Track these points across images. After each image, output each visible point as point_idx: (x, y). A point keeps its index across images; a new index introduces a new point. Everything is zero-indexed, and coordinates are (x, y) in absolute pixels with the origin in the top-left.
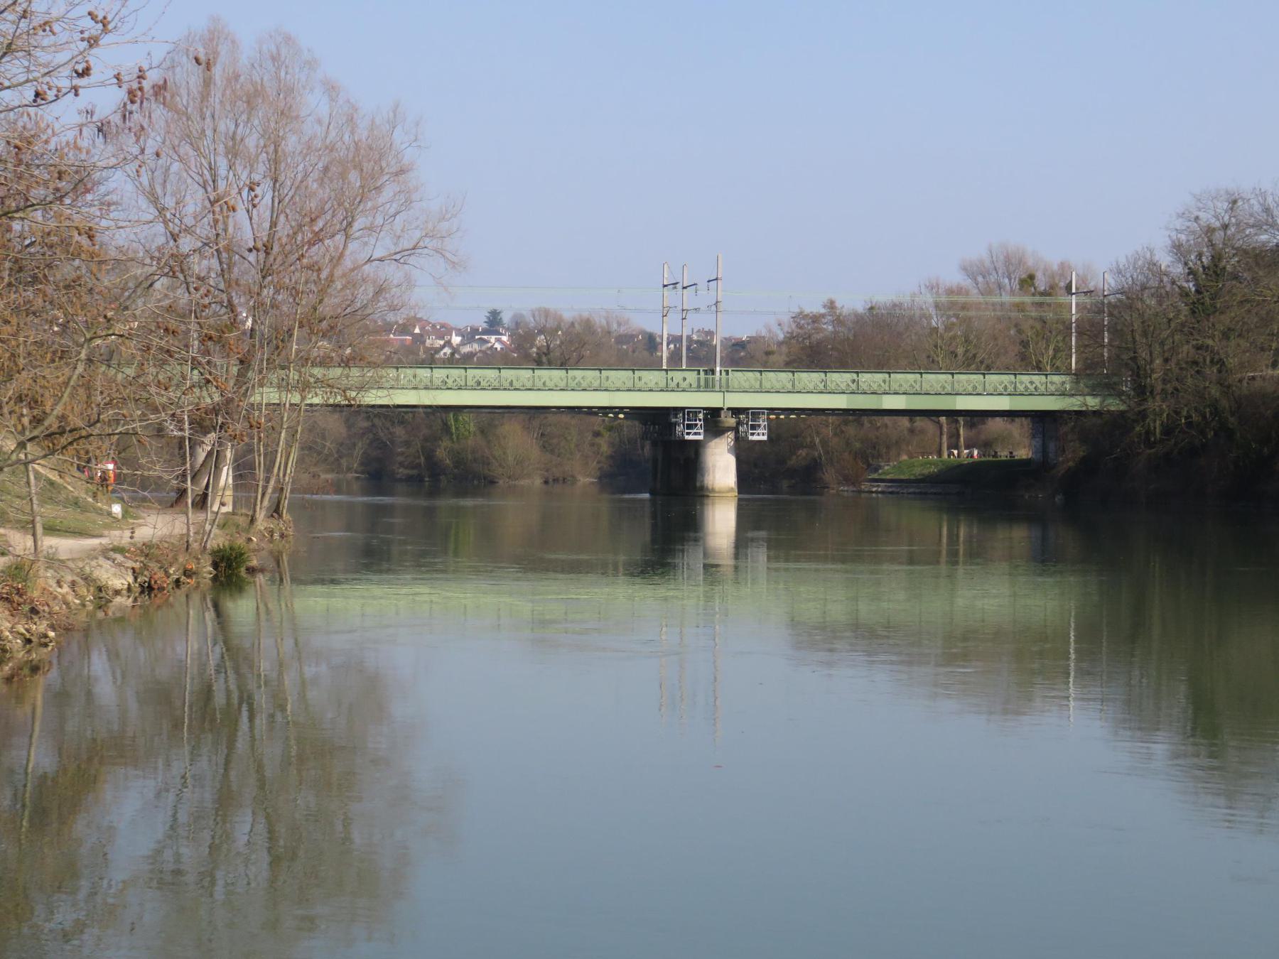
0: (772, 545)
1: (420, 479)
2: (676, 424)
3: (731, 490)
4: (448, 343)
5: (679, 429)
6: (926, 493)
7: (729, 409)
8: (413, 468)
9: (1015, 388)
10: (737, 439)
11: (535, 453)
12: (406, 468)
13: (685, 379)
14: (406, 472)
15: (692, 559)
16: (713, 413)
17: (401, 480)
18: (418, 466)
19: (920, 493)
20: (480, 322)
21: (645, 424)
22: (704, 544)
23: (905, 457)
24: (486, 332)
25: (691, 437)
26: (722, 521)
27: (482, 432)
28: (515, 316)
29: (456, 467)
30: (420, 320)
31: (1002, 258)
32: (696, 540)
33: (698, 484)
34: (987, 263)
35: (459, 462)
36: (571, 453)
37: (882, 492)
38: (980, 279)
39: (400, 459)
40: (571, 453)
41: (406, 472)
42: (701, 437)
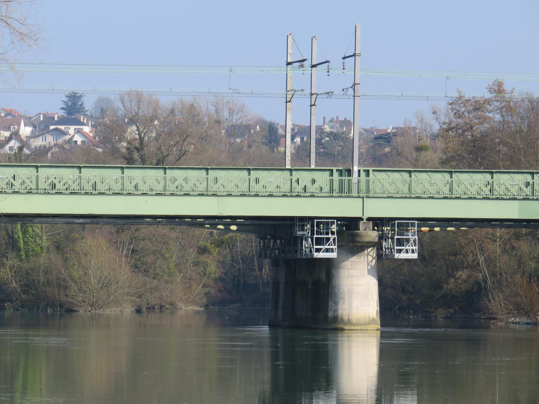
2: (302, 238)
3: (372, 321)
4: (16, 135)
7: (369, 219)
10: (379, 257)
11: (124, 274)
16: (349, 225)
21: (263, 238)
24: (62, 121)
27: (58, 248)
28: (100, 101)
29: (24, 292)
33: (330, 314)
35: (28, 285)
36: (170, 275)
42: (333, 255)
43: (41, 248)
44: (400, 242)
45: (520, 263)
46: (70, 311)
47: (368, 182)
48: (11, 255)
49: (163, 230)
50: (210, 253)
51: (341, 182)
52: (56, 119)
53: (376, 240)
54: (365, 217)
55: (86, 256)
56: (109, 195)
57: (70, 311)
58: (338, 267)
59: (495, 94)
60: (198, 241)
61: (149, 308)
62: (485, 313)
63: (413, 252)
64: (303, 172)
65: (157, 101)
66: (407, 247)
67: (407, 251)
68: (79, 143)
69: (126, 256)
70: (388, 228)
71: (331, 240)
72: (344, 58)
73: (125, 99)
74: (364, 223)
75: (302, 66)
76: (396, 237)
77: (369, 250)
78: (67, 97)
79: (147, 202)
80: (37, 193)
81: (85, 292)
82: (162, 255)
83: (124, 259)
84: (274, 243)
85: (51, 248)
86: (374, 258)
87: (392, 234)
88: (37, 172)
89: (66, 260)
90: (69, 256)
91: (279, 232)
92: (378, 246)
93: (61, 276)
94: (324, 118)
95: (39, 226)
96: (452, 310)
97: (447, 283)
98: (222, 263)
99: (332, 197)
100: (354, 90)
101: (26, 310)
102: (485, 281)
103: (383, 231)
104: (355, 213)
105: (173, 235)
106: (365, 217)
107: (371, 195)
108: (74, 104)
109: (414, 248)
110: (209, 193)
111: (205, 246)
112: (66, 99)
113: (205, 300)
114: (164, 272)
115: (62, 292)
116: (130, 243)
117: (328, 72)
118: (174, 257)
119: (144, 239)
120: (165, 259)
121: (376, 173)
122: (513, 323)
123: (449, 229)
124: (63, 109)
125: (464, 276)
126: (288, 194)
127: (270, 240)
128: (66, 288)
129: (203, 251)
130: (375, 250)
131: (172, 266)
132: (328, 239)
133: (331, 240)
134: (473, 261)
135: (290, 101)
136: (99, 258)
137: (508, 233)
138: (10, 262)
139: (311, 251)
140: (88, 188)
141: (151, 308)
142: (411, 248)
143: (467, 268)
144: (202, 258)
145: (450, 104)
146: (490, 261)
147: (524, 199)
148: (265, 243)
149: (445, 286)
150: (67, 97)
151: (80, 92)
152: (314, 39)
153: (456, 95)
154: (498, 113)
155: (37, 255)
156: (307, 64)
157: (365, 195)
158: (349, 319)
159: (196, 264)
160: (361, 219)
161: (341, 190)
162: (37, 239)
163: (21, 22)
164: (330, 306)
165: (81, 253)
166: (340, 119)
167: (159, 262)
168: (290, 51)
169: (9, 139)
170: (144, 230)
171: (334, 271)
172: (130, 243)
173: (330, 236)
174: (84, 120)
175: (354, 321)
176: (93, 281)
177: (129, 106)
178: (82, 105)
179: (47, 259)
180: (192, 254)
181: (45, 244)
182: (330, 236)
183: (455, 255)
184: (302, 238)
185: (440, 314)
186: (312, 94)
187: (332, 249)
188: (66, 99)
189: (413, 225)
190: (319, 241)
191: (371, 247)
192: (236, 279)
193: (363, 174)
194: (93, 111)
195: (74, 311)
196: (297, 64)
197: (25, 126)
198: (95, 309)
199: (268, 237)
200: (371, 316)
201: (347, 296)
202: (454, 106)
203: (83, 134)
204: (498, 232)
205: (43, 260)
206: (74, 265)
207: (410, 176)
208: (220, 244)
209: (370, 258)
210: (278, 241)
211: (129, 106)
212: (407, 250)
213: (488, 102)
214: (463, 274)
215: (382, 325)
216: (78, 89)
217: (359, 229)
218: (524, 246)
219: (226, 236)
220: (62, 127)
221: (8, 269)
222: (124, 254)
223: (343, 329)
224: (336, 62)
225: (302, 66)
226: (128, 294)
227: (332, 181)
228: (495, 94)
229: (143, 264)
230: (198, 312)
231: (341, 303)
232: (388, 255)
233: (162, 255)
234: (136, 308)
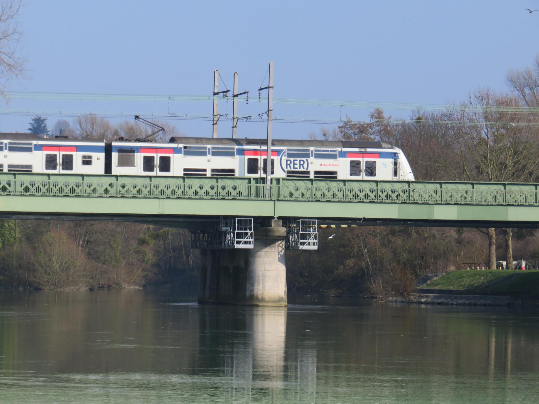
2: (225, 233)
3: (280, 300)
6: (475, 305)
7: (279, 218)
10: (287, 248)
11: (81, 261)
16: (262, 223)
19: (470, 305)
20: (25, 129)
21: (194, 233)
26: (271, 330)
28: (59, 123)
32: (246, 345)
33: (248, 293)
36: (116, 261)
37: (432, 303)
38: (527, 91)
42: (251, 246)
43: (15, 239)
44: (304, 237)
45: (396, 254)
46: (38, 289)
47: (278, 188)
49: (111, 226)
50: (148, 244)
51: (257, 189)
53: (285, 234)
54: (276, 217)
55: (51, 246)
56: (73, 197)
57: (38, 289)
59: (376, 120)
60: (138, 234)
61: (99, 287)
62: (368, 293)
63: (314, 244)
64: (227, 180)
65: (108, 123)
66: (309, 241)
67: (309, 244)
70: (295, 225)
71: (249, 234)
72: (260, 90)
73: (82, 122)
74: (275, 221)
75: (226, 96)
76: (301, 232)
77: (279, 242)
78: (33, 120)
79: (102, 203)
80: (15, 195)
81: (49, 274)
82: (110, 245)
83: (80, 248)
84: (203, 236)
85: (23, 239)
86: (283, 249)
87: (297, 230)
88: (15, 178)
89: (35, 249)
90: (37, 245)
92: (286, 239)
93: (31, 261)
95: (13, 221)
96: (341, 291)
97: (337, 269)
98: (157, 252)
100: (268, 115)
102: (368, 269)
103: (290, 227)
104: (270, 214)
105: (119, 230)
106: (276, 217)
107: (280, 199)
108: (39, 126)
109: (315, 241)
110: (443, 202)
111: (144, 239)
112: (32, 122)
113: (143, 282)
114: (112, 258)
116: (86, 236)
117: (247, 100)
118: (120, 248)
119: (96, 232)
120: (113, 248)
121: (284, 181)
122: (391, 301)
123: (342, 226)
124: (30, 129)
125: (352, 264)
126: (214, 197)
127: (200, 234)
128: (34, 271)
129: (143, 242)
130: (284, 243)
131: (118, 254)
132: (247, 234)
133: (249, 234)
134: (358, 252)
135: (216, 124)
136: (61, 248)
137: (386, 231)
139: (233, 243)
140: (522, 200)
141: (101, 287)
142: (312, 241)
143: (353, 257)
144: (142, 248)
145: (340, 127)
146: (372, 253)
147: (402, 203)
148: (195, 237)
149: (336, 271)
150: (33, 120)
152: (236, 74)
153: (345, 119)
154: (378, 135)
155: (11, 245)
156: (230, 94)
157: (276, 199)
158: (262, 297)
159: (137, 252)
160: (273, 218)
161: (257, 195)
162: (12, 232)
163: (9, 55)
164: (247, 287)
165: (46, 243)
167: (108, 251)
168: (216, 84)
170: (97, 225)
172: (86, 236)
173: (248, 231)
175: (267, 299)
176: (56, 266)
177: (85, 127)
178: (45, 126)
180: (134, 245)
181: (18, 235)
182: (248, 231)
183: (344, 247)
184: (225, 233)
185: (332, 293)
186: (234, 118)
187: (250, 241)
188: (32, 122)
189: (314, 223)
190: (239, 235)
191: (280, 240)
192: (168, 265)
193: (274, 182)
194: (54, 132)
195: (40, 289)
196: (222, 94)
198: (57, 288)
199: (199, 232)
200: (280, 295)
201: (261, 278)
202: (343, 129)
204: (378, 229)
205: (16, 248)
206: (41, 252)
207: (312, 184)
208: (156, 237)
209: (280, 249)
210: (206, 235)
211: (85, 127)
212: (309, 243)
213: (370, 126)
214: (350, 262)
215: (288, 303)
216: (40, 112)
217: (271, 226)
218: (398, 241)
219: (161, 231)
222: (81, 244)
223: (258, 306)
224: (254, 93)
225: (226, 96)
227: (249, 188)
228: (376, 120)
229: (96, 252)
230: (139, 290)
231: (256, 284)
232: (294, 247)
233: (110, 245)
234: (90, 287)
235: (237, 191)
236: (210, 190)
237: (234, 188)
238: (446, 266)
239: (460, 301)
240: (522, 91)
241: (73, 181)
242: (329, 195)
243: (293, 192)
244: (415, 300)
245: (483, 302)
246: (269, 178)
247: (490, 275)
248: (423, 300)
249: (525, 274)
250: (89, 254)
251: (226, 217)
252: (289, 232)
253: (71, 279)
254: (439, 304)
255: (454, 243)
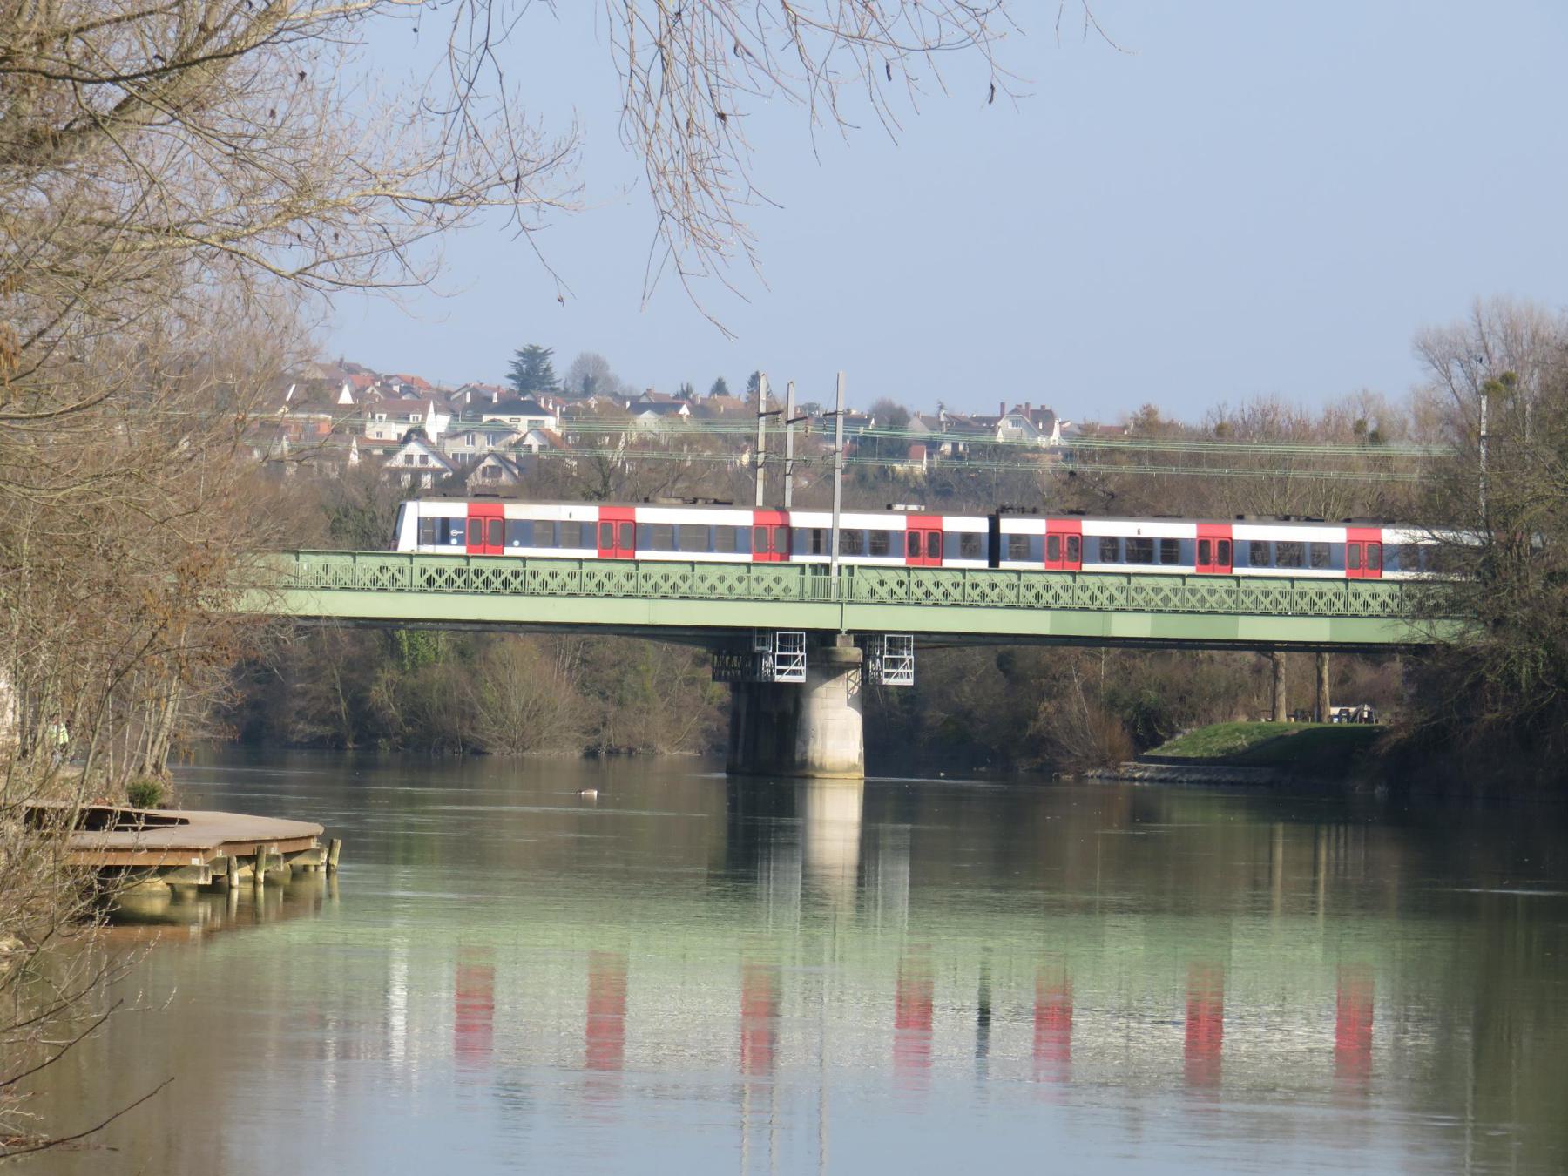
0: (917, 854)
1: (338, 743)
2: (762, 655)
3: (852, 768)
4: (418, 433)
5: (768, 664)
6: (1217, 783)
7: (849, 632)
8: (324, 722)
9: (1346, 604)
10: (865, 680)
11: (564, 696)
12: (311, 722)
13: (777, 580)
14: (308, 729)
15: (781, 879)
16: (821, 640)
17: (300, 746)
18: (334, 718)
19: (1208, 782)
20: (498, 377)
21: (719, 654)
22: (805, 852)
23: (1242, 719)
24: (511, 405)
25: (784, 678)
26: (836, 816)
27: (462, 653)
28: (582, 362)
29: (409, 722)
30: (353, 370)
31: (1498, 327)
32: (792, 845)
33: (798, 757)
34: (1472, 339)
35: (415, 712)
36: (646, 699)
37: (1151, 780)
38: (1456, 369)
39: (299, 703)
40: (646, 699)
41: (308, 729)
42: (801, 679)
48: (389, 664)
52: (495, 401)
54: (844, 630)
58: (809, 695)
68: (535, 449)
69: (570, 669)
78: (520, 354)
91: (733, 648)
93: (466, 699)
94: (1003, 405)
99: (802, 601)
101: (410, 751)
104: (832, 624)
106: (844, 630)
108: (533, 368)
112: (517, 359)
115: (467, 723)
124: (511, 376)
138: (386, 676)
141: (613, 752)
150: (520, 354)
151: (544, 347)
160: (838, 632)
166: (1032, 407)
169: (406, 440)
171: (804, 701)
174: (547, 403)
176: (515, 705)
178: (548, 369)
179: (440, 673)
188: (517, 359)
193: (845, 572)
197: (436, 412)
203: (544, 434)
205: (438, 674)
209: (851, 684)
220: (506, 418)
221: (383, 686)
223: (813, 777)
226: (568, 729)
235: (783, 585)
236: (736, 584)
237: (777, 580)
238: (1231, 714)
239: (1195, 777)
240: (1447, 371)
241: (507, 567)
242: (937, 593)
243: (877, 587)
244: (1127, 775)
245: (1230, 777)
246: (835, 565)
247: (1256, 732)
248: (1137, 775)
249: (1338, 731)
250: (583, 684)
251: (762, 630)
252: (866, 656)
253: (545, 735)
254: (1161, 781)
255: (1247, 673)
